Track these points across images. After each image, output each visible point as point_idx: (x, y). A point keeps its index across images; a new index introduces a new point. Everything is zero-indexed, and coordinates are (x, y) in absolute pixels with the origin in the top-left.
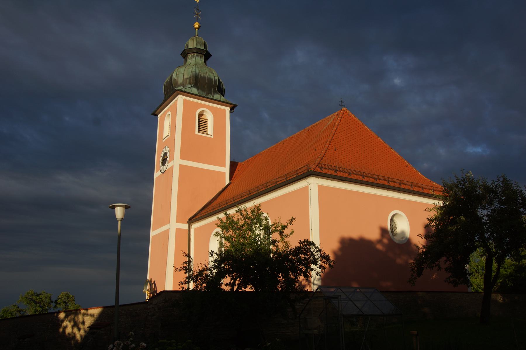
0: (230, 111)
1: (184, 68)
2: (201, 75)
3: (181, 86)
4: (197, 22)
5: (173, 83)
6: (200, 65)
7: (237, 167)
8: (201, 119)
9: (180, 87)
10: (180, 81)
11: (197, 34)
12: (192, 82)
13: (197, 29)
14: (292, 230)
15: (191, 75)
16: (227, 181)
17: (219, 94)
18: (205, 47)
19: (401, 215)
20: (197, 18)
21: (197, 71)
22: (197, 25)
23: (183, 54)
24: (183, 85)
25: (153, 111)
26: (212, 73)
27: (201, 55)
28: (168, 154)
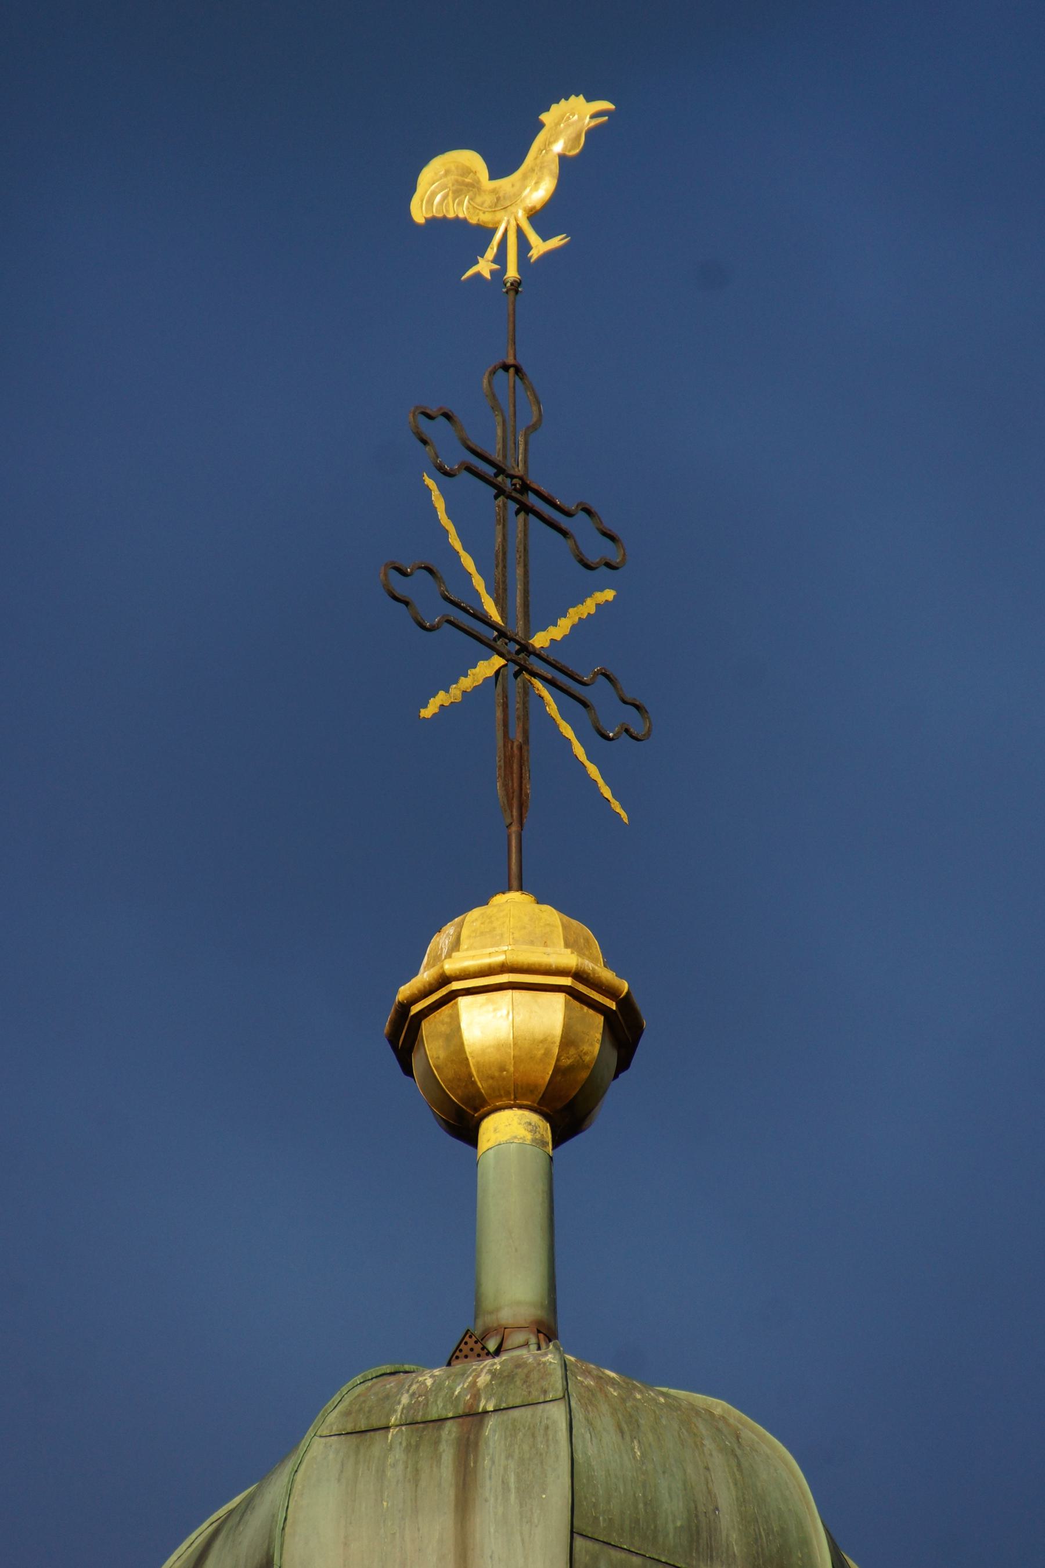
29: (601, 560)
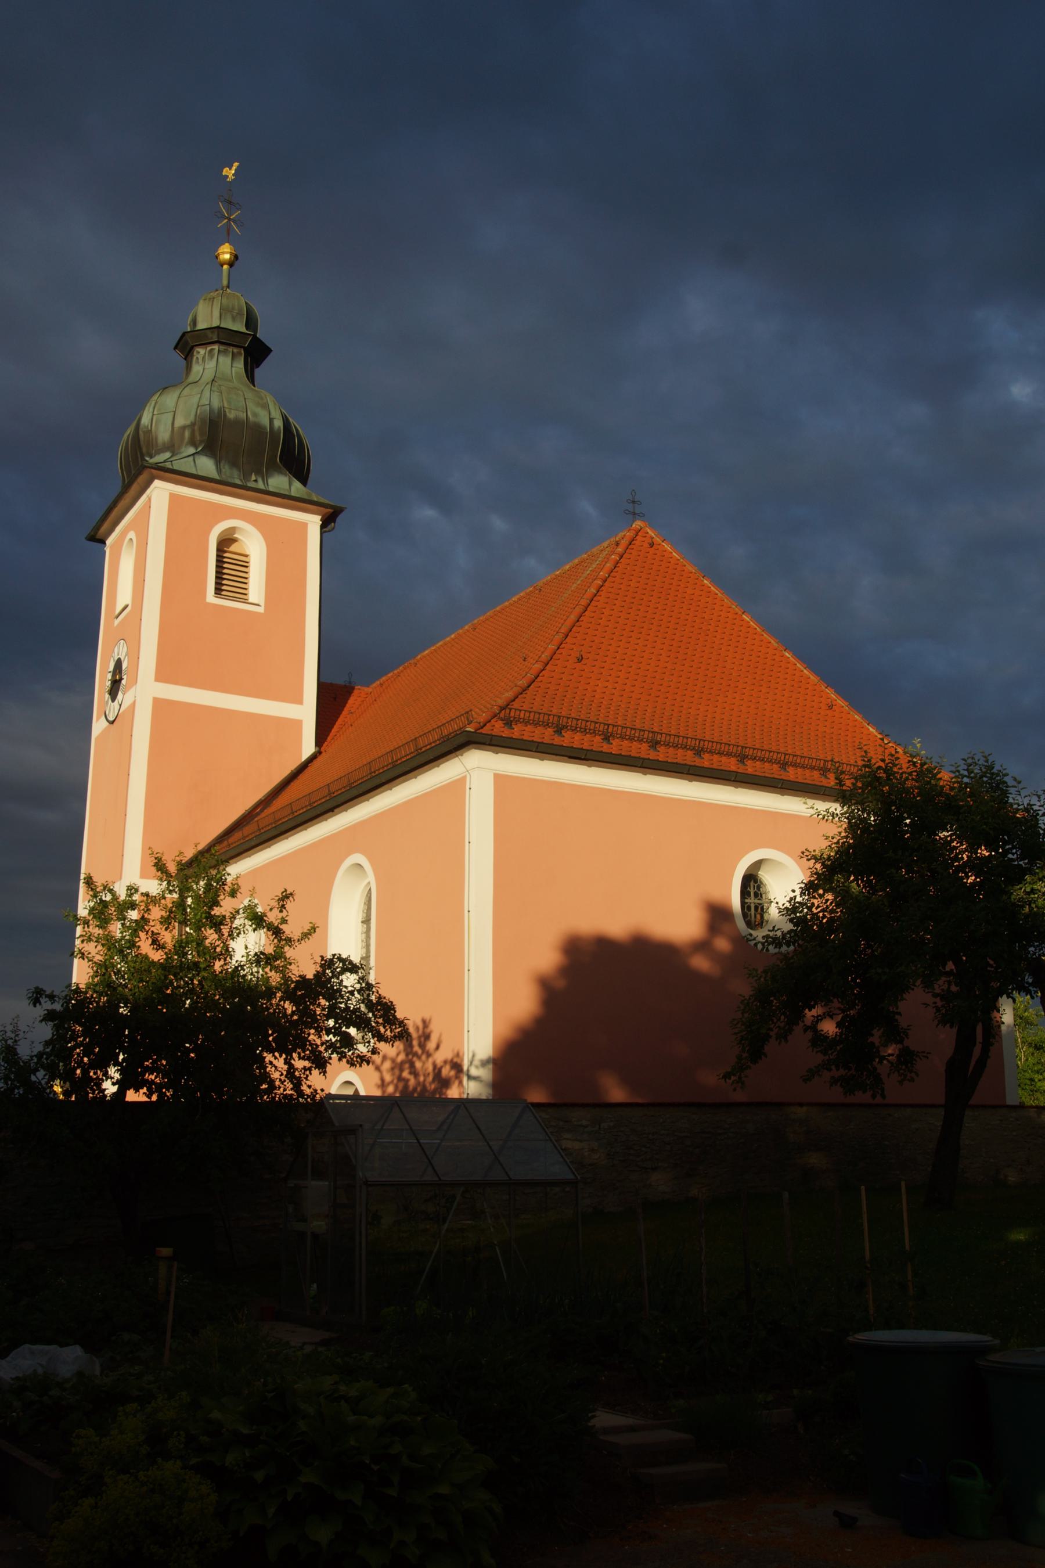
0: (322, 527)
2: (228, 414)
3: (166, 451)
5: (142, 443)
6: (231, 381)
8: (226, 555)
9: (162, 455)
10: (163, 434)
11: (225, 282)
12: (198, 437)
13: (225, 267)
14: (311, 925)
16: (308, 748)
17: (285, 475)
18: (251, 321)
19: (780, 863)
21: (216, 404)
22: (225, 253)
23: (179, 347)
24: (172, 447)
25: (87, 530)
26: (265, 406)
27: (236, 350)
28: (124, 666)
29: (576, 733)
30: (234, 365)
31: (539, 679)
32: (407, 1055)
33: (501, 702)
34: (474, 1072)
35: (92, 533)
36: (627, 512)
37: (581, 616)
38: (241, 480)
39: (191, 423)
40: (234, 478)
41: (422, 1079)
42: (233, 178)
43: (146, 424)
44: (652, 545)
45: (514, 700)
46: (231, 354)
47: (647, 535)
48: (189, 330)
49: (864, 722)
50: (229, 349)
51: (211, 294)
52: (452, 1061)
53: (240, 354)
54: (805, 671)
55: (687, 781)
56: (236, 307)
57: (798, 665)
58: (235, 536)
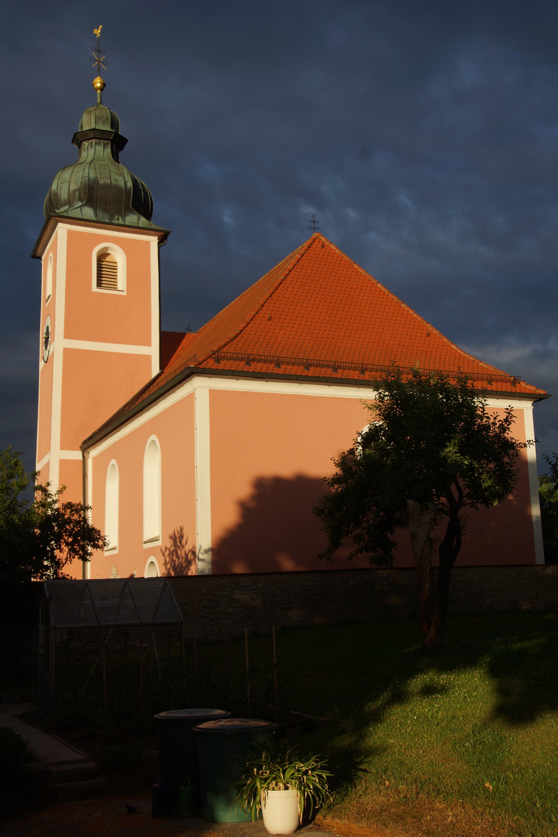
0: (159, 243)
1: (71, 170)
4: (99, 77)
6: (104, 160)
7: (183, 342)
9: (64, 207)
10: (64, 195)
11: (99, 101)
12: (83, 196)
13: (98, 91)
15: (81, 183)
16: (155, 370)
17: (136, 214)
18: (114, 124)
20: (99, 68)
21: (92, 175)
23: (74, 141)
24: (69, 203)
26: (122, 175)
27: (105, 142)
30: (105, 151)
31: (243, 332)
32: (175, 547)
33: (215, 348)
34: (201, 556)
35: (33, 254)
36: (310, 228)
37: (273, 293)
38: (109, 219)
39: (79, 188)
40: (105, 218)
41: (180, 560)
42: (100, 35)
43: (54, 190)
44: (323, 247)
45: (225, 346)
46: (103, 144)
47: (321, 241)
48: (80, 131)
49: (449, 343)
50: (102, 141)
51: (90, 109)
52: (192, 550)
53: (108, 144)
54: (414, 315)
55: (327, 386)
56: (105, 116)
57: (410, 311)
58: (108, 252)
